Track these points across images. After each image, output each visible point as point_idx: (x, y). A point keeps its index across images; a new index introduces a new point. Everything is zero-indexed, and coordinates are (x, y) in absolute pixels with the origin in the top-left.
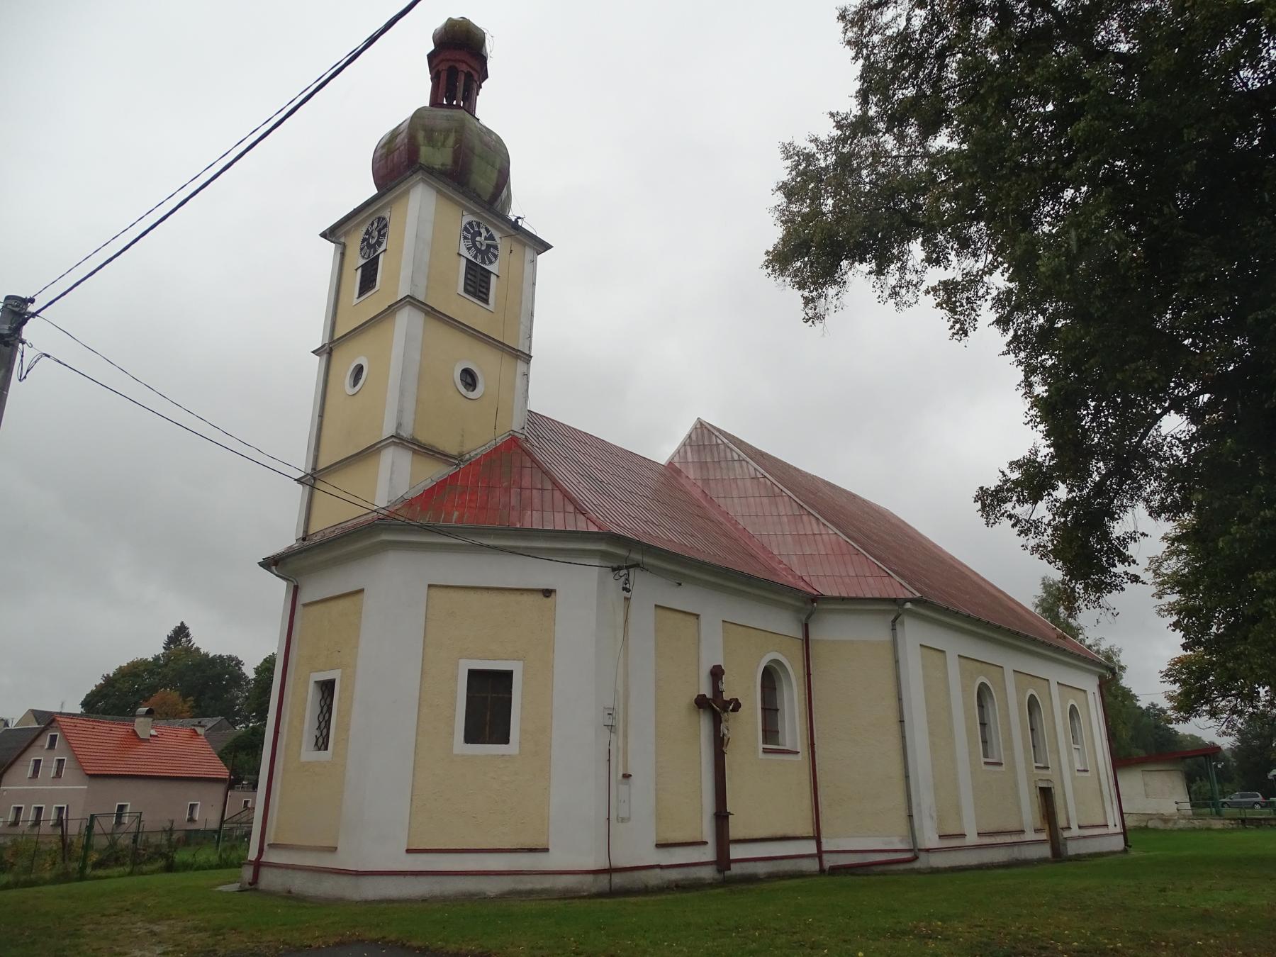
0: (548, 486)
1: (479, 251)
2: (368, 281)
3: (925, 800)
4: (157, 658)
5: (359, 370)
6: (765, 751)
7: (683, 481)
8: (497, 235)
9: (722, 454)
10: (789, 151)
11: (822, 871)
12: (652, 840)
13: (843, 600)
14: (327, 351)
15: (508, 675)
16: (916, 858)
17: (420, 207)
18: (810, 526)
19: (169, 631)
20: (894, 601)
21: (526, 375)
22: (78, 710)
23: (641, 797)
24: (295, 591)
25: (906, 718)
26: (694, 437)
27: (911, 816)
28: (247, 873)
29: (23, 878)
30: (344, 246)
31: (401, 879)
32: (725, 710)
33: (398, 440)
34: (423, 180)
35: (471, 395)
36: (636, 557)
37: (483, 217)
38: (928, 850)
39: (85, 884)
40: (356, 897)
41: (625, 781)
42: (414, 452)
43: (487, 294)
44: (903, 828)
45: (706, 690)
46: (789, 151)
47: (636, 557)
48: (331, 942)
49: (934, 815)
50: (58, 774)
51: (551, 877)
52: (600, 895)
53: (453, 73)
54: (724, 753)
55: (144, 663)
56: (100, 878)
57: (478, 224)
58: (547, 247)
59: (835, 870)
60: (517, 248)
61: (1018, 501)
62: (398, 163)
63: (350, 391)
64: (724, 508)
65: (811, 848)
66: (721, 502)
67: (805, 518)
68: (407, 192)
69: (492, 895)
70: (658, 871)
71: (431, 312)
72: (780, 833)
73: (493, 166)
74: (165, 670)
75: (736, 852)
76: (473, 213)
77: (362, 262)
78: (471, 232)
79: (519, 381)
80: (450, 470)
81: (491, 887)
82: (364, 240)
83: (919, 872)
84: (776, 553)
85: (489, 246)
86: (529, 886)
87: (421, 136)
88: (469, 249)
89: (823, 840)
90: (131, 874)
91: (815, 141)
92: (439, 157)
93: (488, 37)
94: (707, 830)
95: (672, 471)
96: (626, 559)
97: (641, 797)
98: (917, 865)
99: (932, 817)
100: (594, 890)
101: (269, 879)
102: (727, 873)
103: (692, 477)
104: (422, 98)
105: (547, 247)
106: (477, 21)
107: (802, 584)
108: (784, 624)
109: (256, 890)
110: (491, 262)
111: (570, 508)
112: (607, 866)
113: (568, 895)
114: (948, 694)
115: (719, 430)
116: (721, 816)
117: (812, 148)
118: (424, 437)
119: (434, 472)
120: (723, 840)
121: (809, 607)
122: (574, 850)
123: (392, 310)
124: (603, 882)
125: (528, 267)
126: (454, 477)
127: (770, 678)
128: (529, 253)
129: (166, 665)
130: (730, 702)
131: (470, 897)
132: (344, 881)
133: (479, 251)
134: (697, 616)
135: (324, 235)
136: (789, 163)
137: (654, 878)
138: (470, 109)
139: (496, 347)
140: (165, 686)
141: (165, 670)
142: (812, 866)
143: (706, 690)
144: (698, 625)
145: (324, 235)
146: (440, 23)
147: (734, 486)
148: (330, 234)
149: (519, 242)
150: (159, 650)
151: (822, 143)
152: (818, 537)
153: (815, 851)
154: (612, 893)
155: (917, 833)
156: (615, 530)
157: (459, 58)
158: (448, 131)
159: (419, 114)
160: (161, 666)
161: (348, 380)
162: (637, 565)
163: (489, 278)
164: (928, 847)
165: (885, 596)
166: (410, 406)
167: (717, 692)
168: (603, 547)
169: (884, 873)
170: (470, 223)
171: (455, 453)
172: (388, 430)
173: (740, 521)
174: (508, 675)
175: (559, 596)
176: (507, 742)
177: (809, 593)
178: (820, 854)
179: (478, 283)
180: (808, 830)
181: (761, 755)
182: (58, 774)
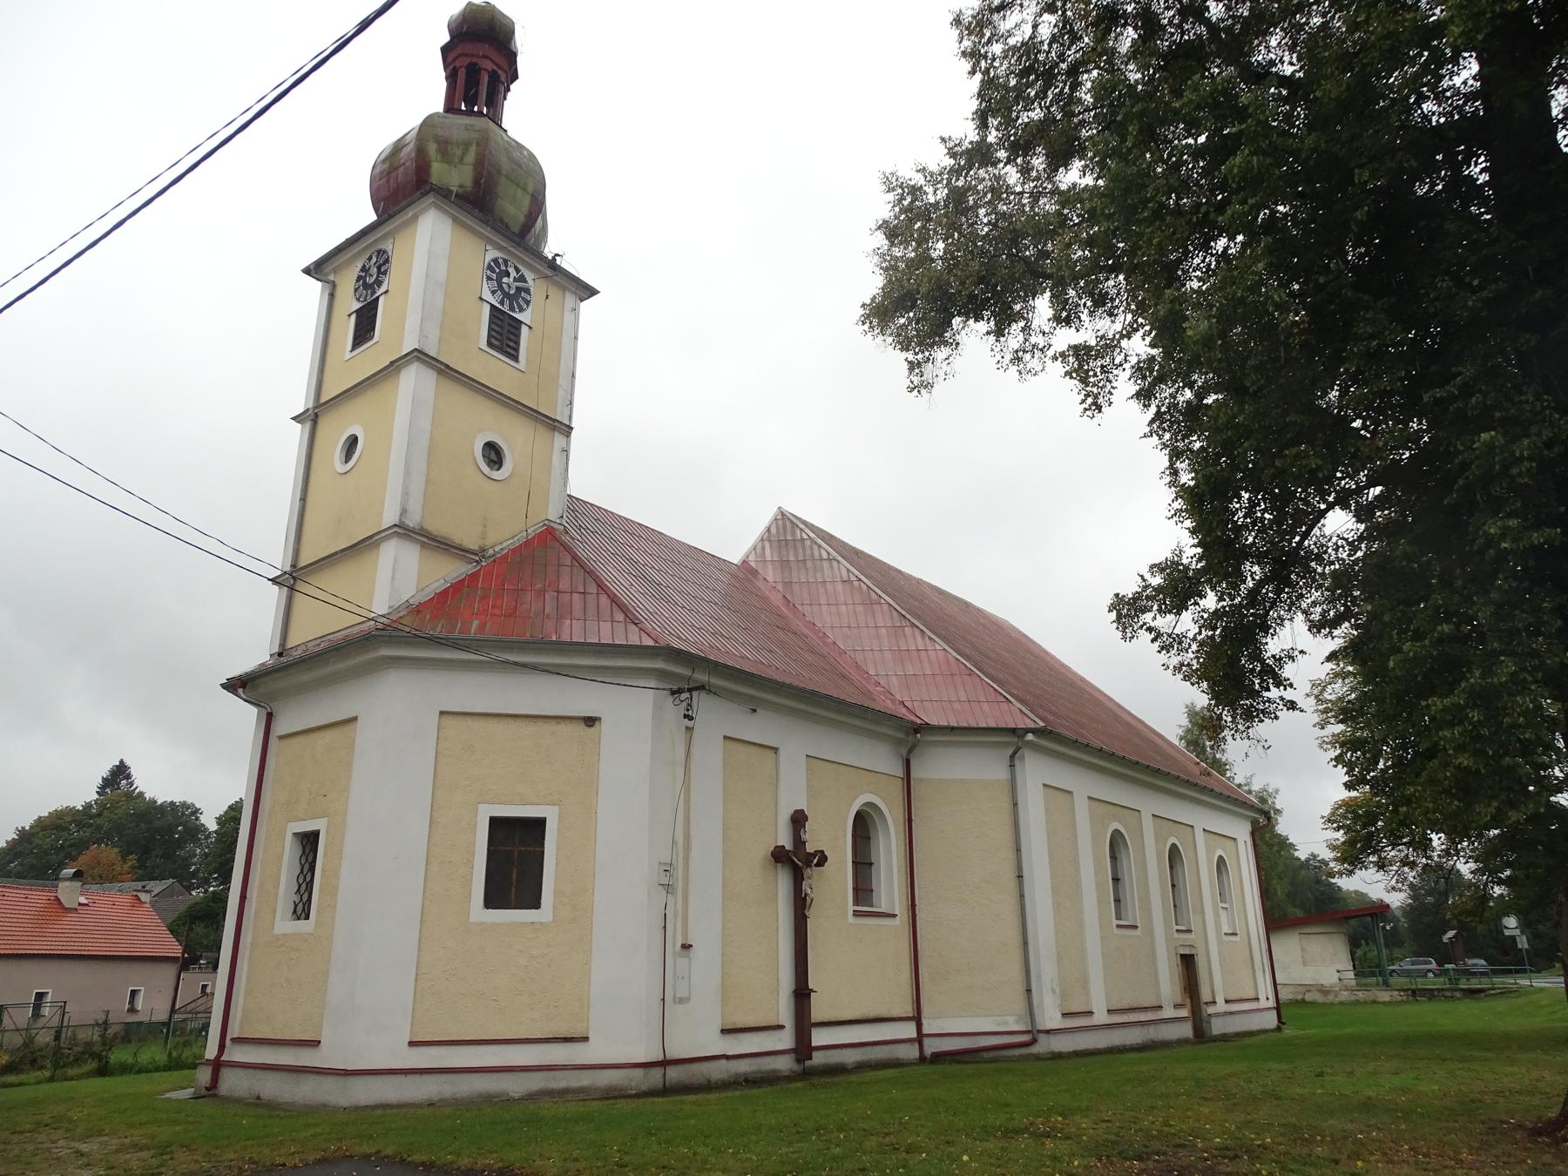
0: (593, 588)
4: (88, 806)
5: (353, 442)
6: (856, 914)
7: (760, 584)
8: (529, 276)
9: (808, 552)
15: (538, 825)
16: (1034, 1041)
20: (1013, 731)
21: (566, 451)
23: (704, 972)
25: (1025, 873)
26: (773, 530)
27: (1029, 991)
28: (204, 1075)
30: (334, 285)
32: (808, 864)
33: (402, 530)
35: (496, 475)
36: (701, 677)
38: (1048, 1032)
42: (423, 545)
43: (517, 350)
44: (1020, 1005)
45: (785, 840)
46: (890, 183)
47: (701, 677)
48: (311, 1159)
52: (652, 1093)
53: (473, 72)
54: (805, 918)
55: (71, 811)
57: (506, 261)
58: (591, 292)
59: (938, 1057)
60: (553, 292)
61: (1160, 610)
62: (402, 183)
65: (909, 1031)
66: (807, 609)
68: (415, 218)
69: (517, 1096)
70: (723, 1062)
71: (445, 371)
72: (872, 1014)
73: (525, 190)
74: (99, 821)
75: (819, 1037)
78: (497, 271)
79: (557, 457)
81: (516, 1086)
83: (1038, 1058)
84: (872, 672)
86: (563, 1085)
88: (493, 292)
89: (925, 1021)
90: (51, 1079)
91: (923, 170)
94: (784, 1012)
95: (746, 573)
97: (704, 972)
98: (1035, 1049)
99: (1054, 991)
100: (644, 1088)
101: (232, 1083)
103: (770, 578)
105: (591, 292)
107: (904, 710)
108: (881, 759)
110: (521, 310)
111: (620, 616)
112: (661, 1058)
113: (612, 1095)
116: (802, 994)
117: (919, 179)
118: (436, 527)
119: (449, 571)
122: (619, 1039)
124: (655, 1077)
125: (568, 316)
126: (473, 577)
127: (864, 825)
128: (570, 299)
129: (99, 815)
130: (814, 855)
131: (489, 1099)
132: (329, 1083)
133: (506, 295)
134: (775, 750)
135: (307, 271)
136: (891, 197)
137: (718, 1071)
141: (99, 821)
142: (911, 1052)
143: (785, 840)
144: (777, 761)
145: (307, 271)
148: (316, 270)
150: (93, 796)
154: (666, 1091)
156: (676, 644)
157: (481, 58)
158: (466, 145)
159: (429, 123)
160: (92, 817)
163: (519, 329)
166: (417, 488)
167: (799, 842)
169: (995, 1060)
170: (495, 261)
172: (390, 517)
174: (538, 825)
175: (605, 727)
178: (920, 1037)
179: (504, 335)
180: (908, 1010)
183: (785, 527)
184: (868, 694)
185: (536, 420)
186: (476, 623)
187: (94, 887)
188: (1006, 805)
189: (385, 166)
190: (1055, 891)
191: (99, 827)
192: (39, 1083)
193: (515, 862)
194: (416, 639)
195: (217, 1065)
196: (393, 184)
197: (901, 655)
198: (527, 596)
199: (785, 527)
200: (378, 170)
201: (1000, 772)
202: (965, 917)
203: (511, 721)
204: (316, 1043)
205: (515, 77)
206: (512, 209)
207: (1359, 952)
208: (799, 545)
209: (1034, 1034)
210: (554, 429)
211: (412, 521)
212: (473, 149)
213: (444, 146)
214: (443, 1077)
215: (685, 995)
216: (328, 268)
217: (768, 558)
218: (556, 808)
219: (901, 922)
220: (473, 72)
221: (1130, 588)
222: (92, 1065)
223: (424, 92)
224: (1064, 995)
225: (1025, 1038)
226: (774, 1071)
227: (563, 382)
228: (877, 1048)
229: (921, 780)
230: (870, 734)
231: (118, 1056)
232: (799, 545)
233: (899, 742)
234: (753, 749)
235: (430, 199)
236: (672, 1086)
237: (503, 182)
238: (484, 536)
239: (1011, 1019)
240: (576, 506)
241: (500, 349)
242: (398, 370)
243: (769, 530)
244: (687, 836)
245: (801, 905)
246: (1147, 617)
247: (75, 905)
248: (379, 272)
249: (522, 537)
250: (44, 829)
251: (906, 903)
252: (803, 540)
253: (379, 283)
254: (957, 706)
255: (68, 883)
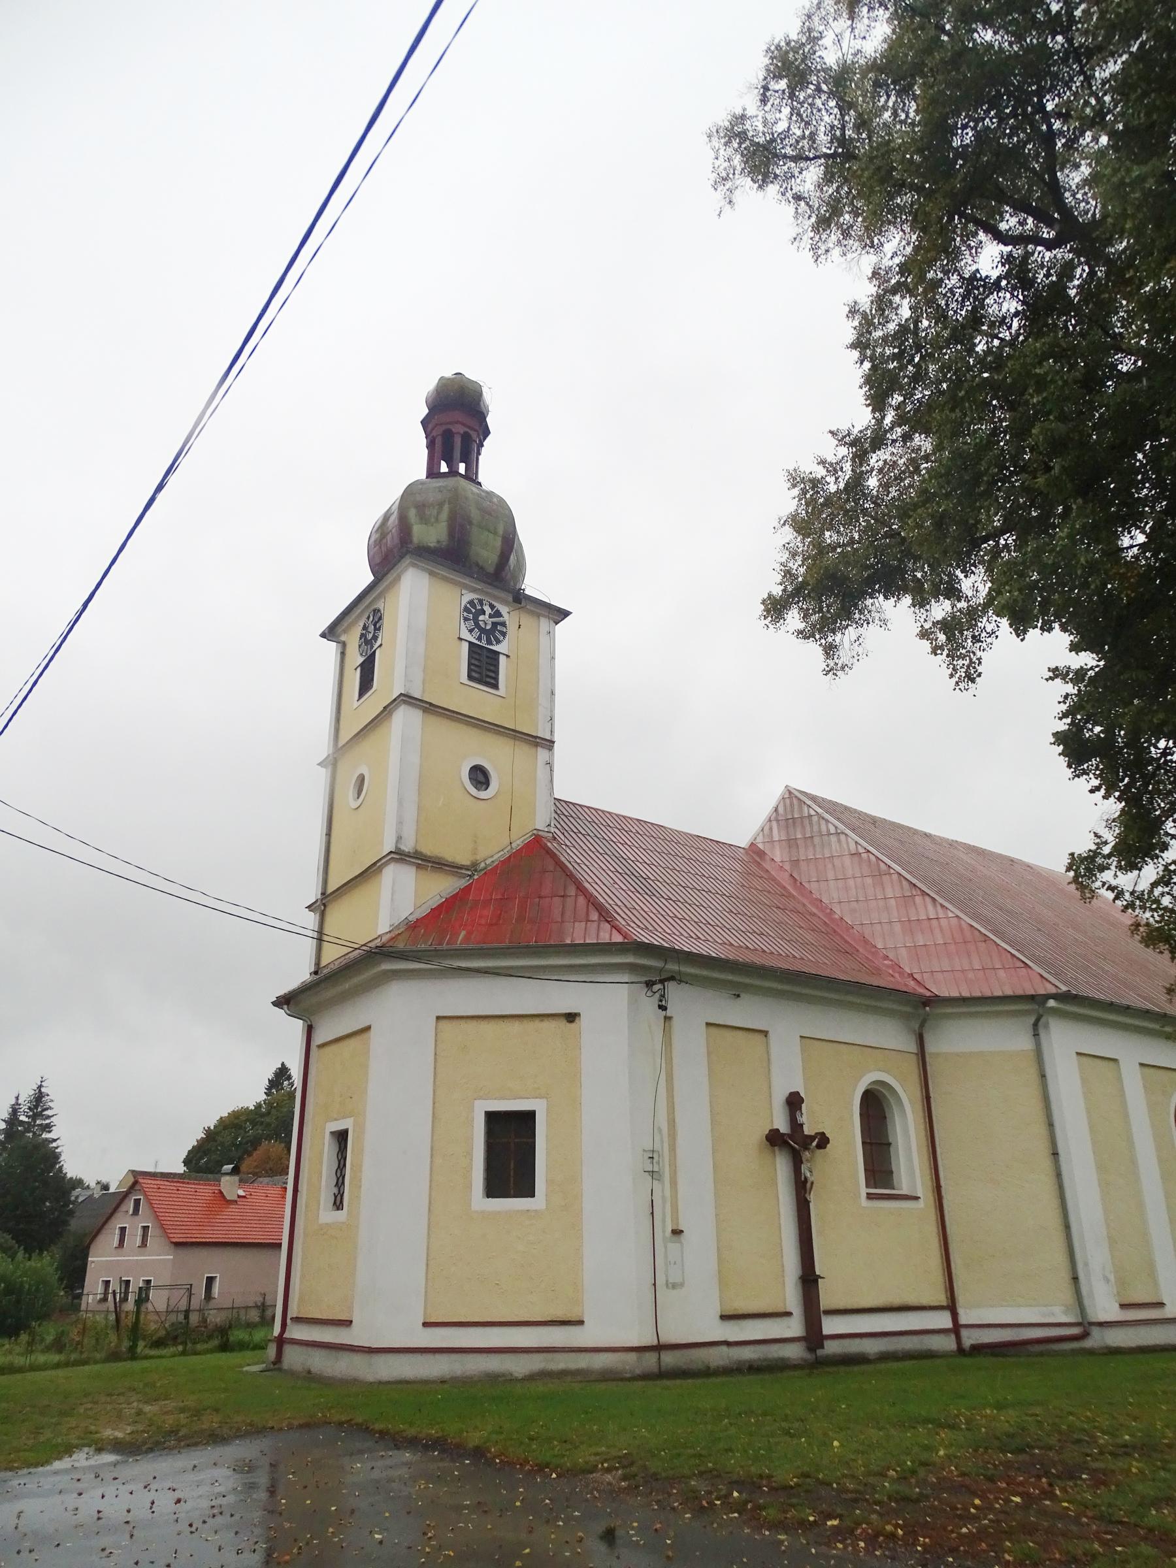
0: (572, 891)
1: (482, 630)
2: (366, 684)
3: (1096, 1259)
4: (258, 1106)
5: (361, 779)
6: (870, 1196)
7: (767, 865)
8: (504, 610)
9: (815, 828)
10: (795, 479)
11: (961, 1351)
12: (716, 1311)
13: (963, 1001)
14: (333, 763)
15: (530, 1116)
16: (1085, 1335)
17: (414, 588)
18: (924, 910)
19: (270, 1074)
20: (1032, 998)
21: (550, 764)
22: (180, 1169)
23: (698, 1256)
24: (310, 1030)
25: (1061, 1151)
26: (781, 810)
27: (1075, 1279)
28: (272, 1351)
29: (73, 1357)
30: (344, 645)
31: (418, 1358)
32: (806, 1147)
33: (399, 856)
34: (414, 565)
35: (483, 794)
36: (672, 967)
37: (487, 594)
38: (1101, 1324)
39: (137, 1365)
40: (370, 1378)
41: (675, 1238)
42: (418, 866)
43: (496, 679)
44: (1067, 1295)
45: (781, 1124)
46: (795, 479)
47: (672, 967)
48: (296, 1423)
49: (1112, 1277)
50: (144, 1244)
51: (588, 1356)
52: (645, 1377)
53: (448, 436)
54: (807, 1203)
55: (246, 1111)
56: (152, 1357)
57: (481, 602)
58: (565, 614)
59: (977, 1349)
60: (526, 620)
61: (1119, 867)
62: (392, 550)
63: (354, 805)
64: (816, 895)
65: (943, 1320)
66: (813, 887)
67: (918, 900)
68: (399, 578)
69: (520, 1376)
70: (724, 1348)
71: (429, 708)
72: (897, 1301)
73: (495, 533)
74: (267, 1119)
75: (830, 1326)
76: (474, 590)
77: (361, 660)
78: (472, 612)
79: (542, 772)
80: (463, 883)
81: (520, 1366)
82: (362, 635)
83: (1091, 1352)
84: (879, 946)
85: (494, 624)
86: (562, 1366)
87: (412, 514)
88: (471, 631)
89: (961, 1311)
90: (184, 1353)
91: (822, 462)
92: (432, 534)
93: (485, 390)
94: (792, 1299)
95: (755, 852)
96: (661, 970)
97: (698, 1256)
98: (1088, 1344)
99: (1107, 1280)
100: (638, 1372)
101: (293, 1358)
102: (820, 1352)
103: (778, 859)
104: (418, 470)
105: (565, 614)
106: (471, 375)
107: (912, 983)
108: (889, 1035)
109: (280, 1370)
110: (498, 642)
111: (594, 916)
112: (655, 1343)
113: (607, 1376)
114: (1126, 1116)
115: (814, 798)
116: (809, 1280)
117: (820, 472)
118: (428, 849)
119: (442, 887)
120: (812, 1311)
121: (921, 1011)
122: (613, 1324)
123: (387, 711)
124: (650, 1360)
125: (544, 639)
126: (466, 890)
127: (875, 1106)
128: (544, 624)
129: (268, 1113)
130: (812, 1138)
131: (493, 1378)
132: (358, 1359)
133: (482, 630)
134: (765, 1033)
135: (323, 635)
136: (796, 492)
137: (717, 1358)
138: (471, 476)
139: (507, 735)
140: (269, 1138)
141: (267, 1119)
142: (947, 1344)
143: (781, 1124)
144: (767, 1044)
145: (323, 635)
146: (431, 385)
147: (830, 866)
148: (330, 633)
149: (532, 613)
150: (261, 1097)
151: (831, 464)
152: (934, 922)
153: (948, 1324)
154: (663, 1374)
155: (1086, 1302)
156: (646, 938)
157: (456, 421)
158: (441, 505)
159: (411, 492)
160: (263, 1115)
161: (351, 792)
162: (672, 978)
163: (497, 660)
164: (1102, 1320)
165: (1020, 992)
166: (411, 814)
167: (796, 1126)
168: (630, 959)
169: (1041, 1354)
170: (471, 602)
171: (468, 863)
172: (389, 846)
173: (837, 909)
174: (530, 1116)
175: (584, 1022)
176: (532, 1194)
177: (921, 996)
178: (957, 1328)
179: (483, 666)
180: (941, 1299)
181: (864, 1202)
182: (144, 1244)
183: (792, 804)
184: (877, 972)
185: (515, 738)
186: (463, 933)
187: (266, 1180)
188: (1032, 1073)
189: (378, 535)
190: (1101, 1168)
191: (269, 1125)
192: (173, 1356)
193: (510, 1155)
194: (402, 956)
195: (281, 1341)
196: (383, 549)
197: (910, 926)
198: (517, 907)
199: (792, 804)
200: (373, 539)
201: (1024, 1043)
202: (997, 1199)
203: (500, 1022)
204: (348, 1323)
205: (487, 432)
206: (486, 552)
207: (78, 1263)
208: (806, 822)
209: (1086, 1326)
210: (537, 745)
211: (407, 847)
212: (446, 507)
213: (421, 507)
214: (454, 1357)
215: (678, 1280)
216: (339, 629)
217: (776, 838)
218: (544, 1101)
219: (926, 1202)
220: (448, 436)
221: (1085, 846)
222: (215, 1342)
223: (411, 460)
224: (1122, 1283)
225: (1075, 1331)
226: (782, 1359)
227: (543, 700)
228: (903, 1339)
229: (937, 1055)
230: (875, 1010)
231: (238, 1335)
232: (806, 822)
233: (906, 1017)
234: (740, 1033)
235: (407, 560)
236: (668, 1370)
237: (475, 531)
238: (475, 851)
239: (1058, 1310)
240: (564, 810)
241: (480, 681)
242: (390, 714)
243: (776, 810)
244: (672, 1123)
245: (801, 1188)
246: (1107, 876)
247: (235, 1198)
248: (376, 629)
249: (506, 854)
250: (225, 1128)
251: (929, 1184)
252: (810, 816)
253: (375, 638)
254: (971, 975)
255: (227, 1178)
